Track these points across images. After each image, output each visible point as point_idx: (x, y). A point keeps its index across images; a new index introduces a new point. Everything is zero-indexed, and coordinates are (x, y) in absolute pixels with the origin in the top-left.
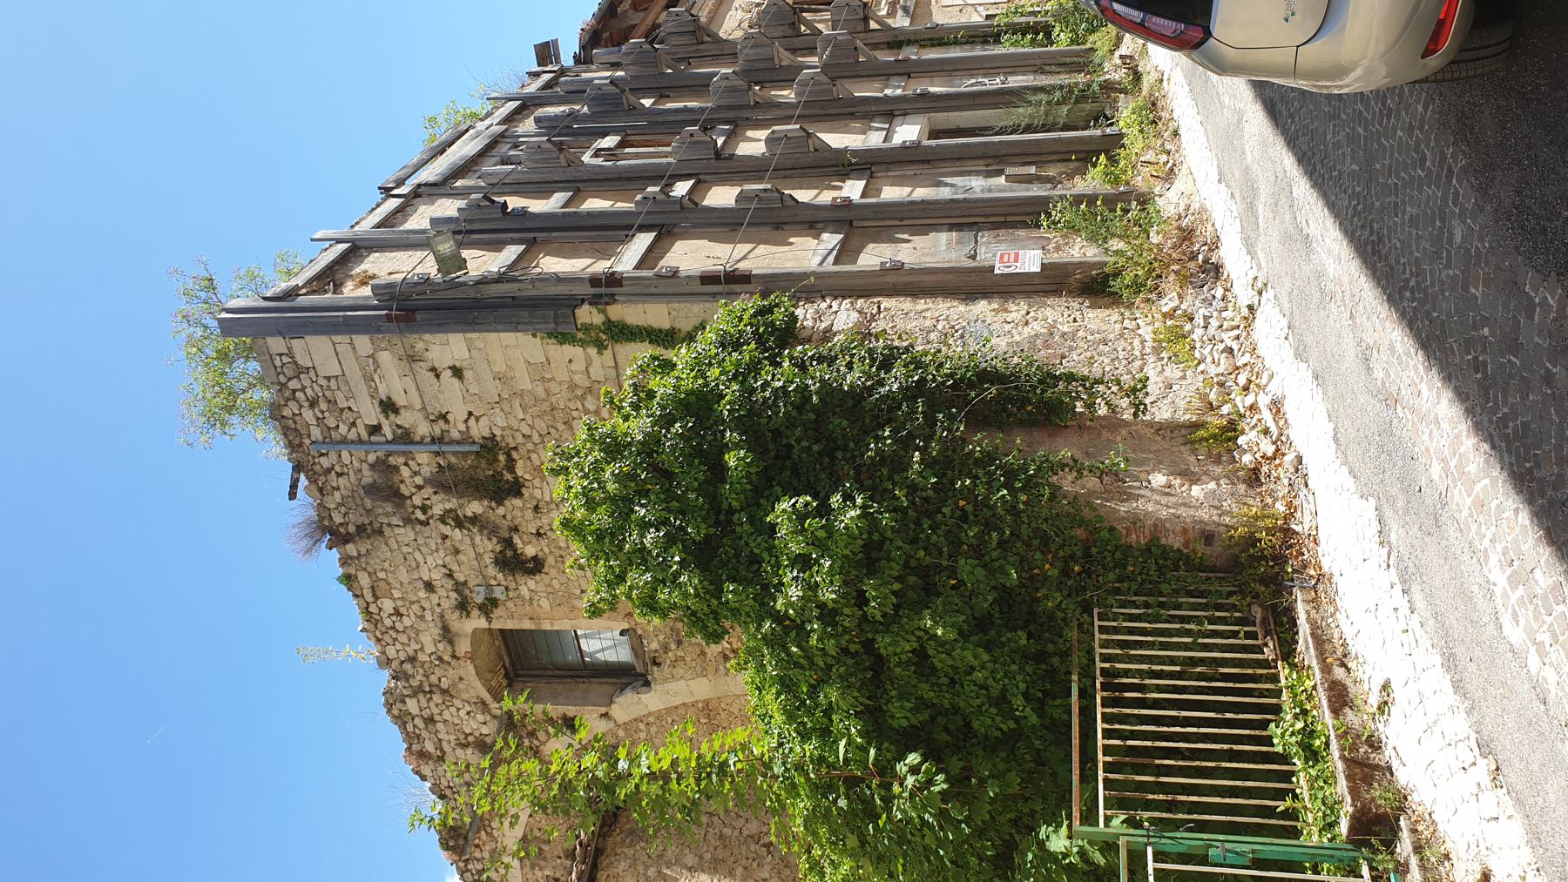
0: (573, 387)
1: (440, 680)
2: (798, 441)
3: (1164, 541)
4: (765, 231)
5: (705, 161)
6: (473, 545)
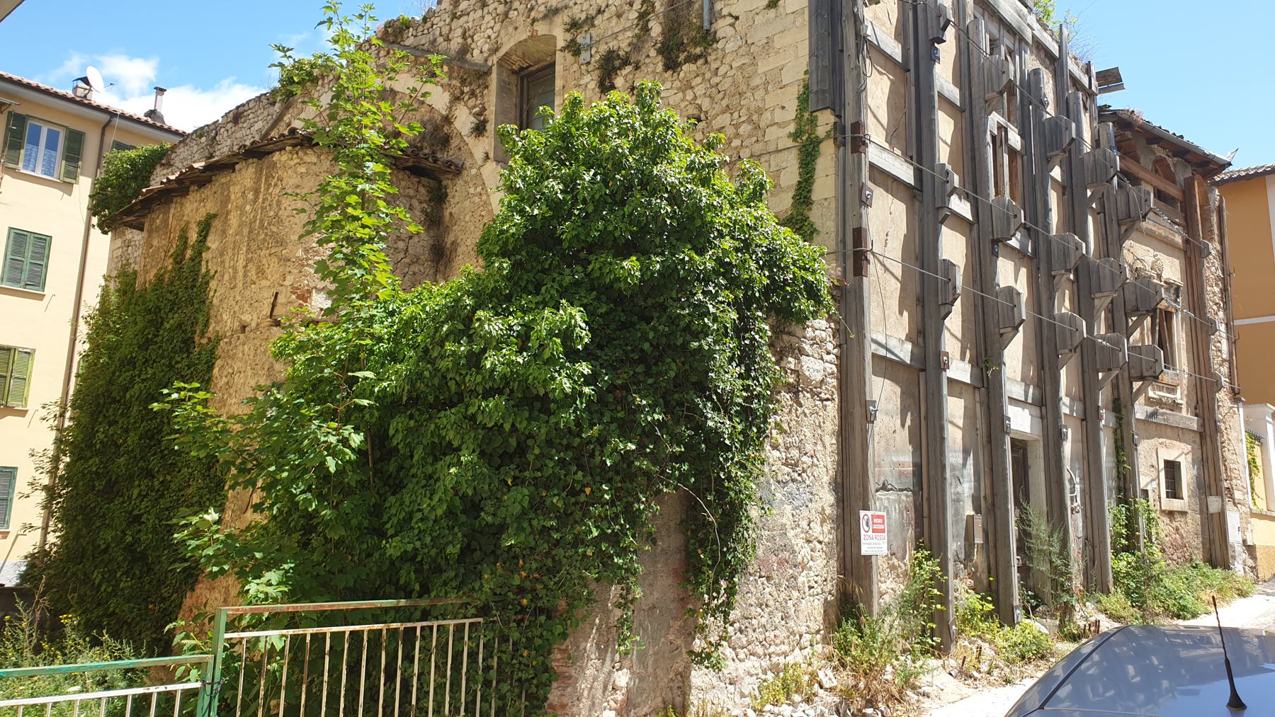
0: (760, 111)
1: (516, 10)
2: (654, 329)
3: (555, 685)
4: (915, 288)
5: (990, 229)
6: (625, 30)
